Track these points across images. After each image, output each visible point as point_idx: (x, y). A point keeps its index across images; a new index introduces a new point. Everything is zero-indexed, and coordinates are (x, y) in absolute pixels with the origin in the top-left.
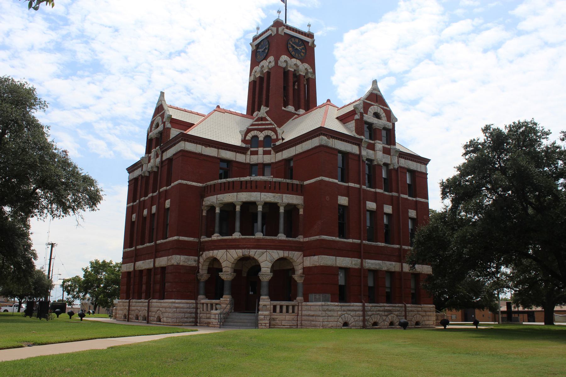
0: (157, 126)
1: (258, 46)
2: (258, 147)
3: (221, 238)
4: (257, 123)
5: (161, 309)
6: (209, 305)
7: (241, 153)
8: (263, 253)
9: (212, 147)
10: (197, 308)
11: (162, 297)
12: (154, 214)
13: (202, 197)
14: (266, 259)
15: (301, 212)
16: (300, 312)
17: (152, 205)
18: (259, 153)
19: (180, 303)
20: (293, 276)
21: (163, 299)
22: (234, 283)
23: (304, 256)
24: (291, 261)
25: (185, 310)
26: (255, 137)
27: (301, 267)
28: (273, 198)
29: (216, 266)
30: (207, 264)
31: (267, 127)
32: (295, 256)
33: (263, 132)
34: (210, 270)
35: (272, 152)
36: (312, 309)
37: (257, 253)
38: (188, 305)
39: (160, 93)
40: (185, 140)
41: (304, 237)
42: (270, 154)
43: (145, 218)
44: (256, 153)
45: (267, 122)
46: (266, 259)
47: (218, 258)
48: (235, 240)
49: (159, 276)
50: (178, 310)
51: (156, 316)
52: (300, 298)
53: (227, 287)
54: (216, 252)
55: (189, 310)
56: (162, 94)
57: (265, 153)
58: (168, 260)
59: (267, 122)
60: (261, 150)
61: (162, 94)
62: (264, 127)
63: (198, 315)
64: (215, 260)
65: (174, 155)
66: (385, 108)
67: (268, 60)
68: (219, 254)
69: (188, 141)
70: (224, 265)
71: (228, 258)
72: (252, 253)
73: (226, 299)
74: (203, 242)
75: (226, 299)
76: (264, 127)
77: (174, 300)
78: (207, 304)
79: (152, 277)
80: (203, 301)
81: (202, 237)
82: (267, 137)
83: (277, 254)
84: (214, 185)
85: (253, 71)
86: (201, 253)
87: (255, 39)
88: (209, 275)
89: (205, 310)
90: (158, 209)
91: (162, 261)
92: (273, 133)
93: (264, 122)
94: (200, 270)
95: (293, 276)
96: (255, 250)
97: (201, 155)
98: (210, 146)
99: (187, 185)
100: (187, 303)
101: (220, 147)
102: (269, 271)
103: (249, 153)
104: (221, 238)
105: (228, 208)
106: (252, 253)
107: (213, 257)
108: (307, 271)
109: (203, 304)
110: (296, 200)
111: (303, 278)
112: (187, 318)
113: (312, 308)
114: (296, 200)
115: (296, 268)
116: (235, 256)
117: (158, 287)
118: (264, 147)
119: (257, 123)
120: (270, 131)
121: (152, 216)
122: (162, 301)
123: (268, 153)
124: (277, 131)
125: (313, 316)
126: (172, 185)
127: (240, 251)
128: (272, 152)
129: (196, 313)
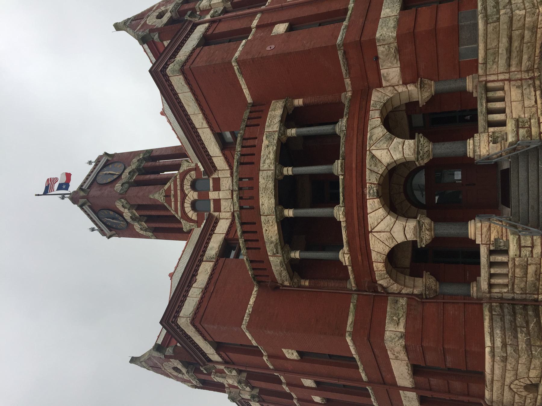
0: (176, 369)
1: (110, 228)
2: (209, 200)
3: (346, 249)
4: (173, 204)
5: (508, 381)
6: (492, 271)
7: (215, 227)
8: (373, 156)
9: (197, 271)
10: (501, 301)
11: (479, 375)
12: (316, 382)
13: (276, 287)
14: (388, 151)
15: (298, 102)
16: (501, 77)
17: (302, 386)
18: (217, 197)
19: (493, 341)
20: (421, 104)
21: (482, 374)
22: (437, 213)
23: (381, 86)
24: (390, 109)
25: (507, 326)
26: (193, 205)
27: (401, 89)
28: (271, 148)
29: (406, 260)
30: (401, 277)
31: (179, 188)
32: (377, 97)
33: (186, 192)
34: (416, 273)
35: (215, 176)
36: (494, 44)
37: (373, 168)
38: (497, 319)
39: (133, 365)
40: (177, 317)
41: (345, 90)
42: (219, 179)
43: (328, 400)
44: (217, 202)
45: (172, 188)
46: (388, 151)
47: (387, 250)
48: (347, 214)
49: (434, 381)
50: (509, 341)
51: (524, 393)
52: (469, 84)
53: (449, 230)
54: (374, 256)
55: (507, 318)
56: (134, 360)
57: (217, 188)
58: (397, 358)
59: (172, 188)
60: (213, 195)
61: (134, 360)
62: (179, 192)
63: (516, 296)
64: (393, 257)
65: (205, 339)
66: (155, 8)
67: (122, 209)
68: (379, 247)
69: (178, 312)
70: (400, 238)
71: (387, 230)
72: (372, 179)
73: (478, 230)
74: (357, 284)
75: (478, 230)
76: (179, 192)
77: (487, 350)
78: (491, 276)
79: (436, 395)
80: (484, 286)
81: (349, 286)
82: (193, 186)
83: (376, 128)
84: (251, 262)
85: (141, 232)
86: (380, 289)
87: (103, 234)
88: (426, 274)
89: (503, 271)
90: (308, 375)
91: (401, 371)
92: (188, 177)
93: (172, 192)
94: (416, 292)
95: (421, 104)
96: (368, 172)
97: (205, 291)
98: (195, 275)
99: (251, 315)
100: (492, 328)
101: (199, 258)
102: (412, 142)
103: (216, 214)
104: (346, 249)
105: (289, 230)
106: (372, 179)
107: (385, 262)
108: (410, 75)
109: (491, 286)
110: (275, 114)
111: (426, 81)
112: (527, 323)
113: (492, 44)
114: (275, 114)
115: (405, 99)
116: (381, 212)
117: (457, 385)
118: (209, 190)
119: (173, 204)
120: (185, 181)
121: (320, 386)
122: (488, 377)
123: (217, 181)
124: (184, 171)
125: (510, 39)
126: (254, 343)
127: (369, 203)
128: (215, 176)
129: (513, 302)
